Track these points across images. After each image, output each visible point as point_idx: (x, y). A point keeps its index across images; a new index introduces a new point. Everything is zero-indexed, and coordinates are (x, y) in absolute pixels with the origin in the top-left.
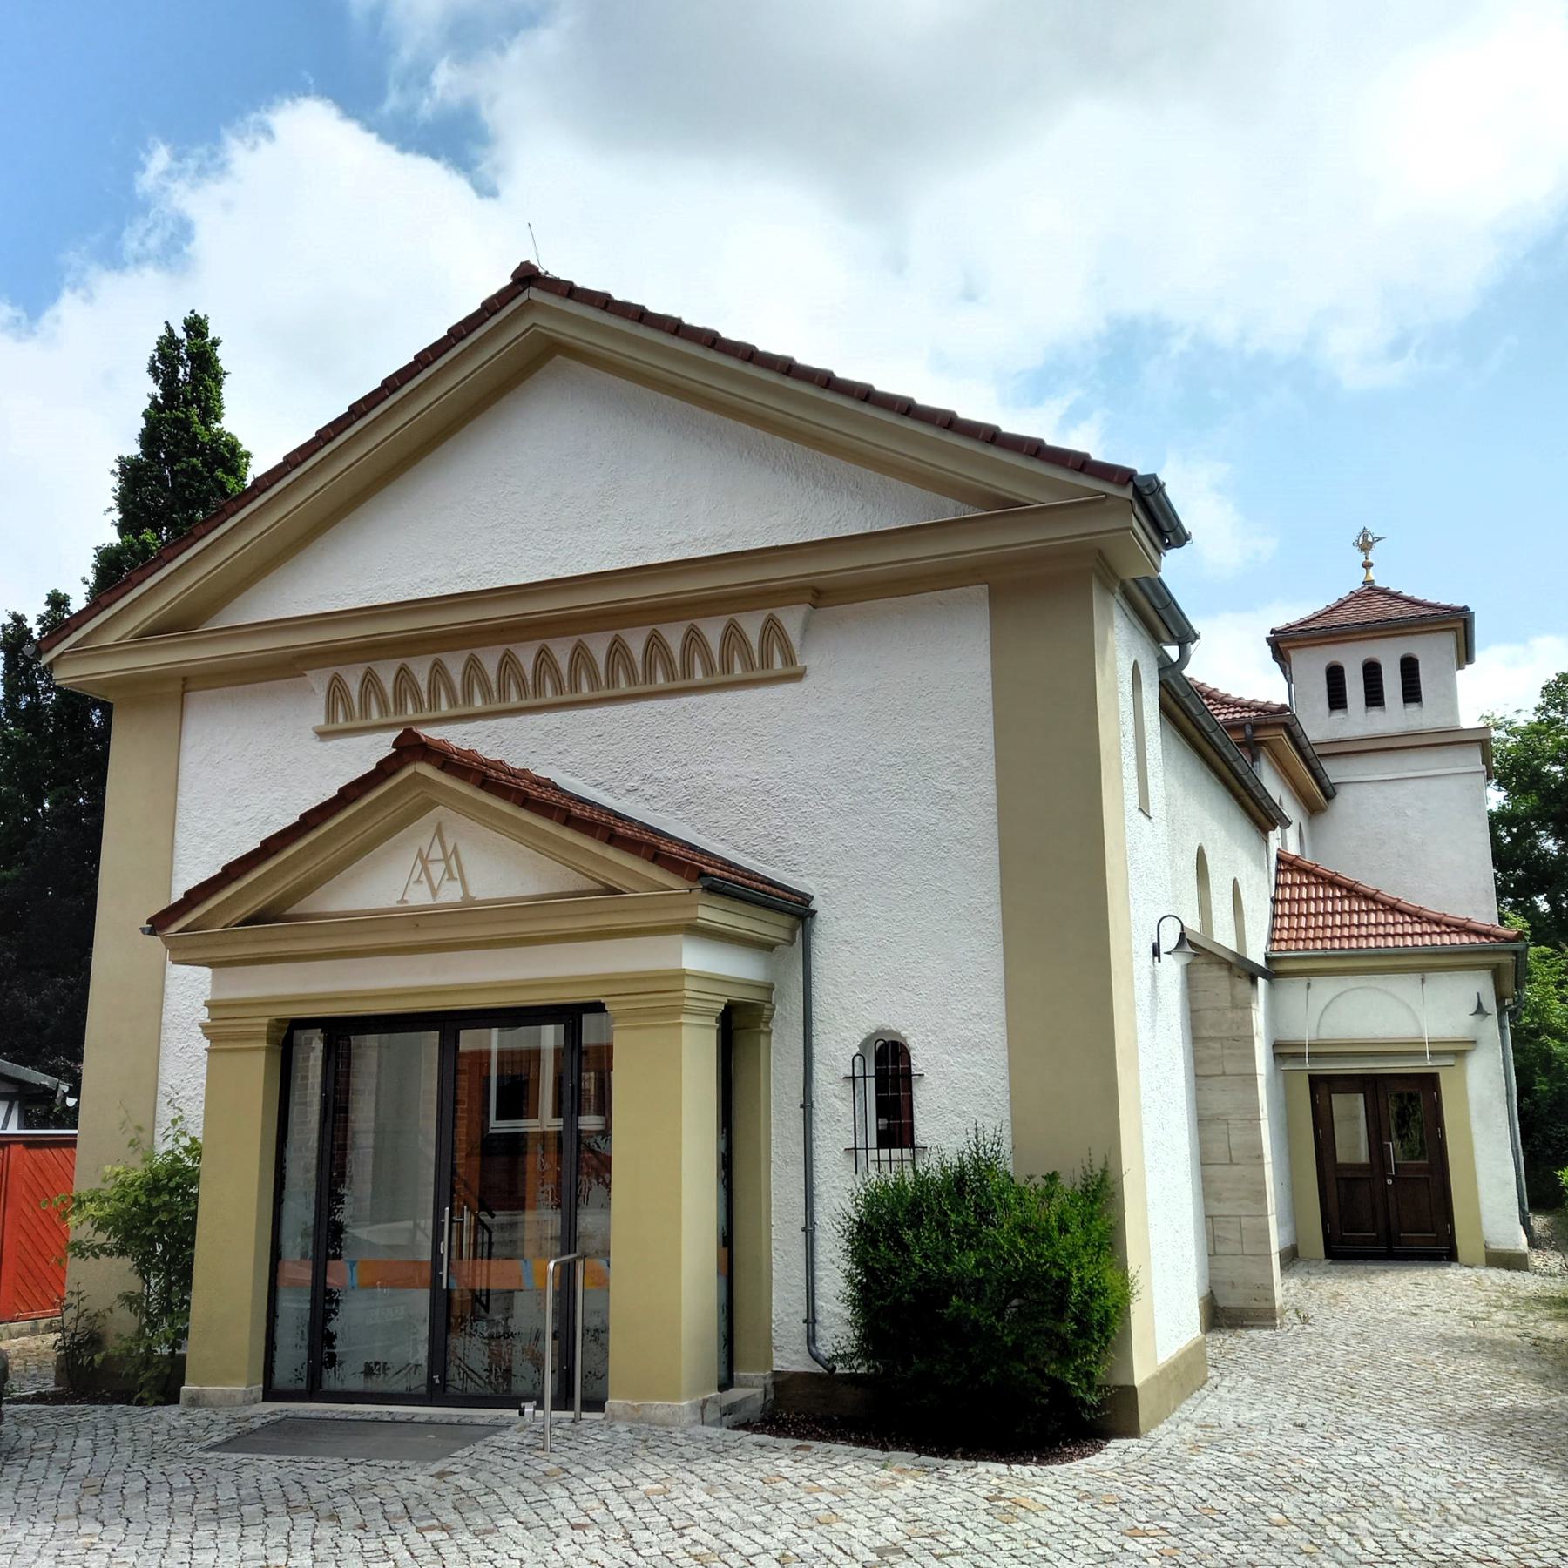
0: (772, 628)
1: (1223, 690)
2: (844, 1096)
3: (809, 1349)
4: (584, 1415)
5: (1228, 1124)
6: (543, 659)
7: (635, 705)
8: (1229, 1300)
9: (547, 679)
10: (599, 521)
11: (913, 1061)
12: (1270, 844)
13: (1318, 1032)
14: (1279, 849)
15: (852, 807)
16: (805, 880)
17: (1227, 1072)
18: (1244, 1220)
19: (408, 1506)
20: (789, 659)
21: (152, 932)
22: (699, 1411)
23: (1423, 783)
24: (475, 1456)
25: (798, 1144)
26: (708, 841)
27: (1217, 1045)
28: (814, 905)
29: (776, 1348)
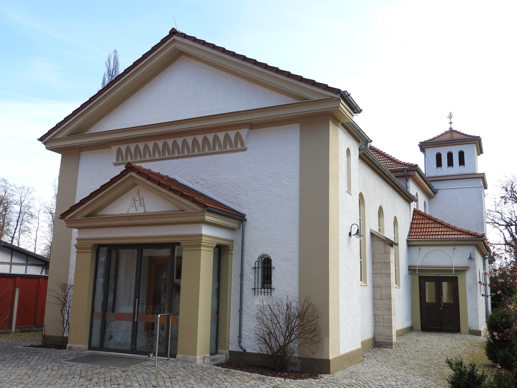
0: (238, 136)
1: (400, 160)
2: (252, 273)
3: (239, 344)
4: (171, 359)
5: (382, 288)
6: (175, 144)
7: (199, 157)
8: (380, 339)
9: (176, 149)
10: (192, 104)
11: (272, 264)
12: (411, 207)
13: (422, 263)
14: (414, 208)
15: (258, 189)
16: (244, 210)
17: (382, 272)
18: (385, 316)
19: (112, 378)
20: (243, 144)
21: (62, 218)
22: (203, 359)
23: (464, 189)
24: (136, 367)
25: (239, 287)
26: (217, 198)
27: (380, 265)
28: (246, 218)
29: (230, 344)
